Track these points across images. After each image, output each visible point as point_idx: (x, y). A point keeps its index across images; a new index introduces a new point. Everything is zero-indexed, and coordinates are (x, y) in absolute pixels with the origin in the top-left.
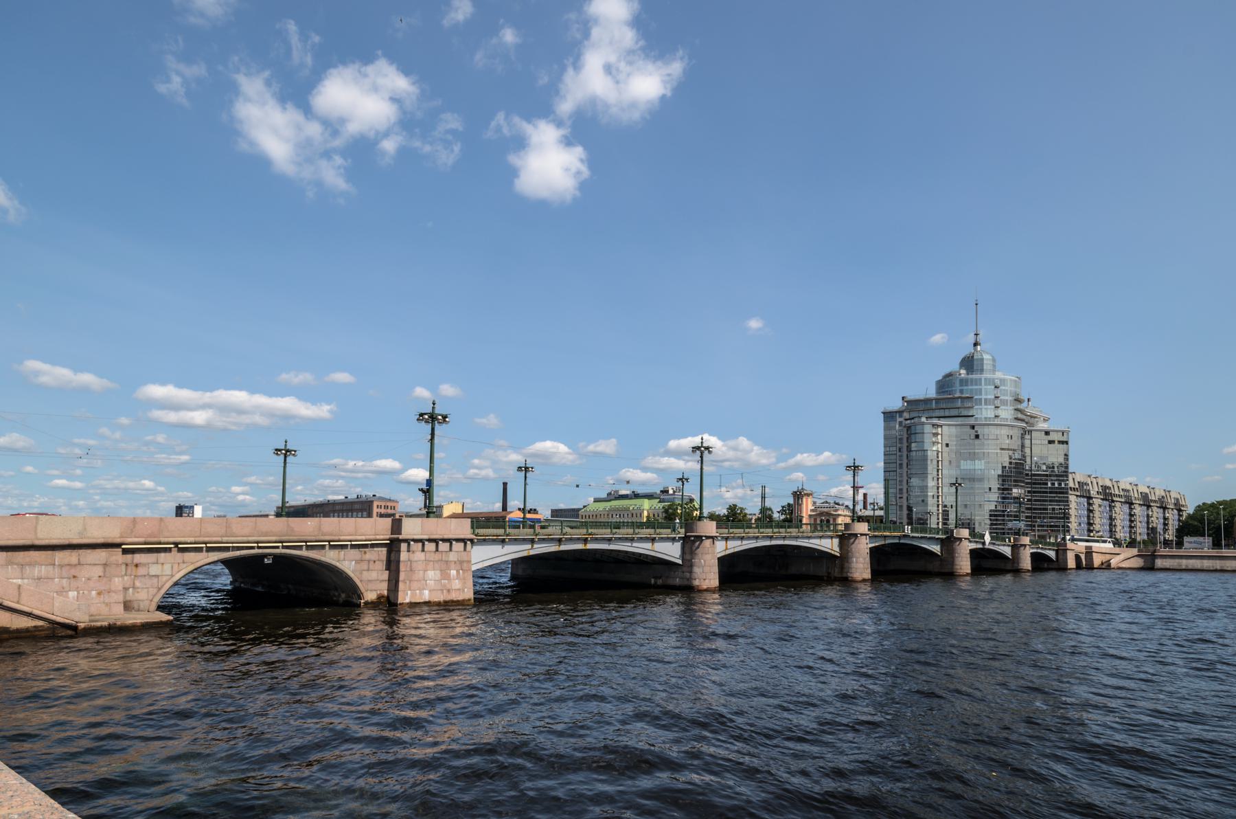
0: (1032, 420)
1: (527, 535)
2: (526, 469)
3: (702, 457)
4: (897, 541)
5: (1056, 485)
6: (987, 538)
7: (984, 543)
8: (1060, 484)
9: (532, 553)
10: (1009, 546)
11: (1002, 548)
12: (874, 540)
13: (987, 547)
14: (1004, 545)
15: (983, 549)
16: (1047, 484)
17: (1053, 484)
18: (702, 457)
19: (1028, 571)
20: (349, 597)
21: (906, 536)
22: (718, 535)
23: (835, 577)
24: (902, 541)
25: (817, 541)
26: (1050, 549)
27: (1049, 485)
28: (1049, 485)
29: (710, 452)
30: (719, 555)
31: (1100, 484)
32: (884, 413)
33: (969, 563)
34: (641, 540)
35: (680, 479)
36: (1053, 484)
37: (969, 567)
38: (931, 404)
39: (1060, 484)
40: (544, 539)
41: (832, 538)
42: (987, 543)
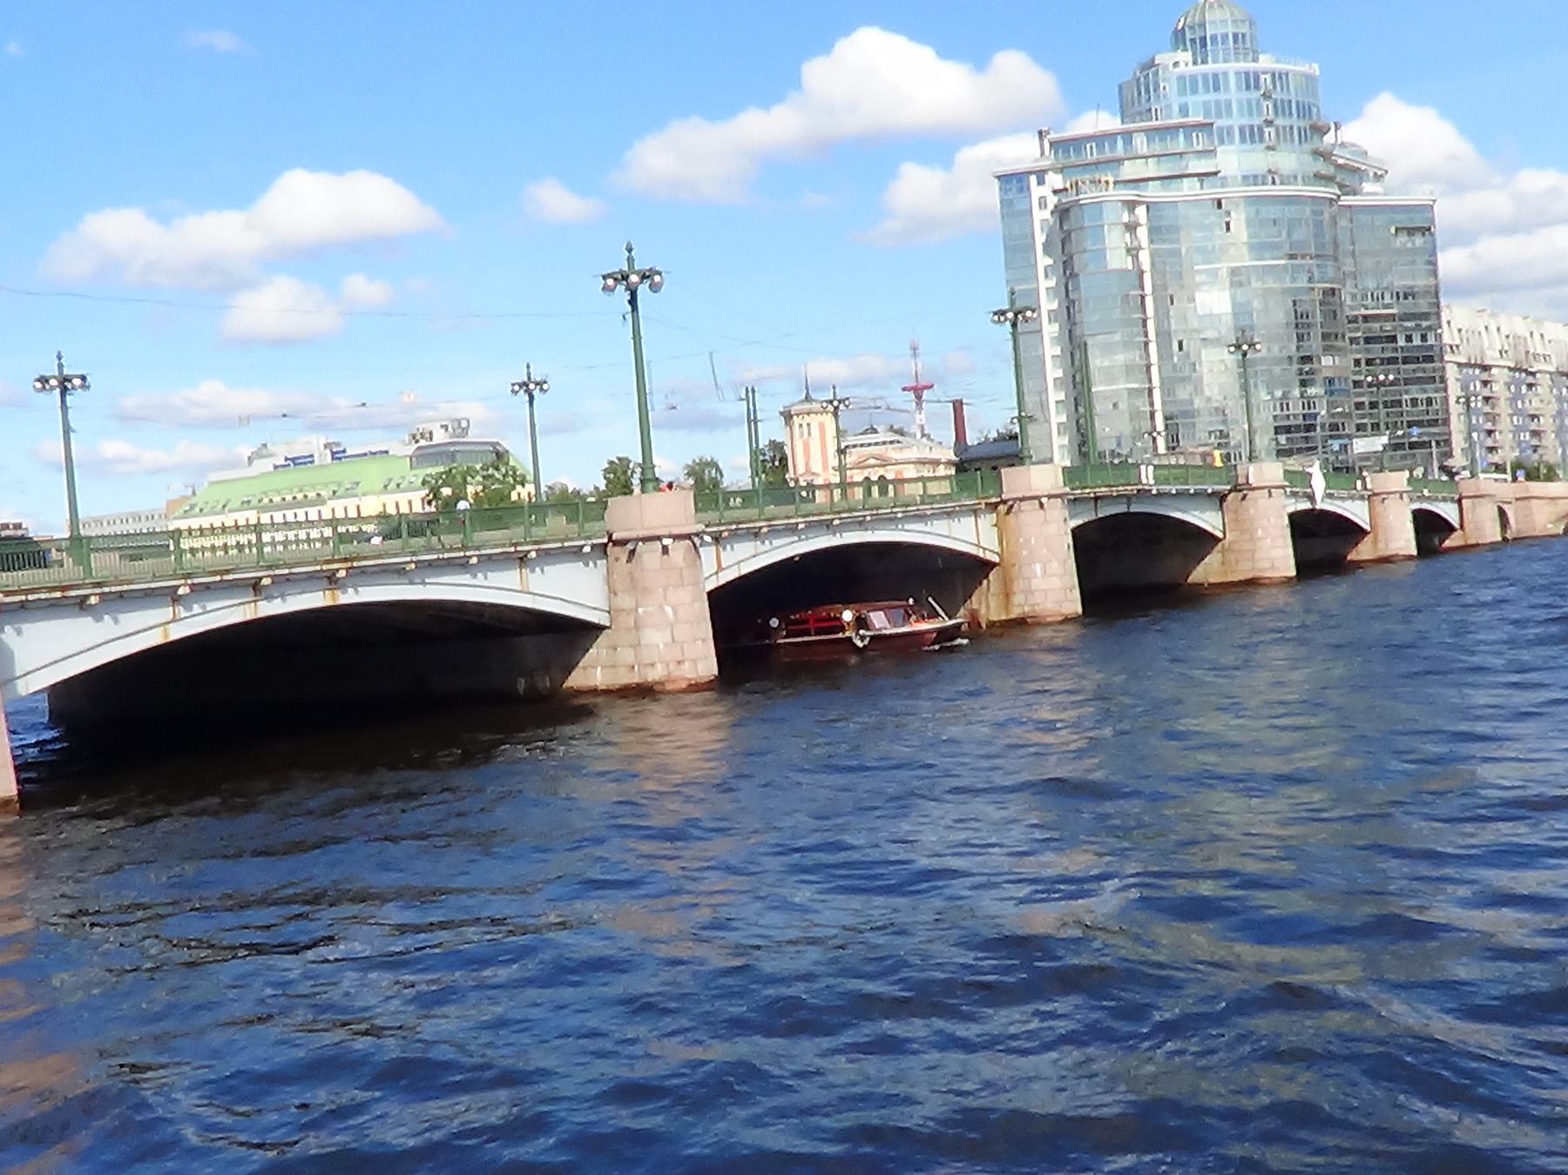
0: (1349, 180)
1: (155, 578)
2: (64, 384)
3: (633, 301)
4: (1122, 509)
5: (1417, 341)
6: (1318, 484)
7: (1311, 498)
8: (1424, 338)
9: (178, 632)
10: (1362, 498)
11: (1348, 504)
12: (1080, 507)
13: (1319, 506)
14: (1352, 498)
15: (1313, 510)
16: (1393, 339)
17: (1409, 339)
18: (633, 301)
19: (1410, 558)
20: (1358, 1021)
21: (1143, 494)
22: (701, 527)
23: (991, 624)
24: (1135, 509)
25: (940, 526)
26: (1444, 500)
27: (1401, 342)
28: (1401, 342)
29: (655, 288)
30: (711, 585)
31: (1504, 331)
32: (999, 177)
33: (1290, 551)
34: (490, 562)
35: (521, 385)
36: (1409, 339)
37: (1292, 561)
38: (1113, 147)
39: (1424, 338)
40: (207, 586)
41: (975, 512)
42: (1319, 495)
